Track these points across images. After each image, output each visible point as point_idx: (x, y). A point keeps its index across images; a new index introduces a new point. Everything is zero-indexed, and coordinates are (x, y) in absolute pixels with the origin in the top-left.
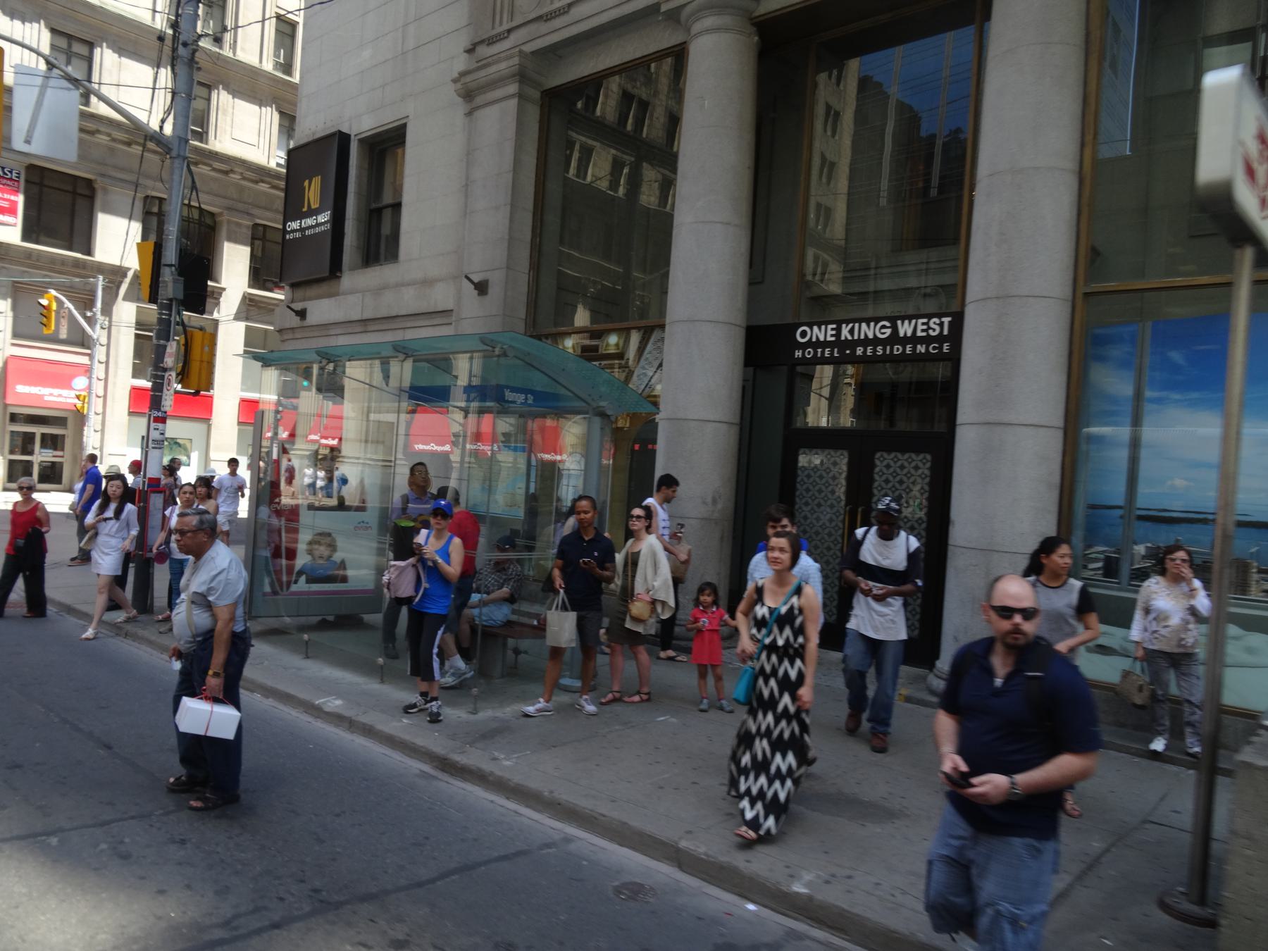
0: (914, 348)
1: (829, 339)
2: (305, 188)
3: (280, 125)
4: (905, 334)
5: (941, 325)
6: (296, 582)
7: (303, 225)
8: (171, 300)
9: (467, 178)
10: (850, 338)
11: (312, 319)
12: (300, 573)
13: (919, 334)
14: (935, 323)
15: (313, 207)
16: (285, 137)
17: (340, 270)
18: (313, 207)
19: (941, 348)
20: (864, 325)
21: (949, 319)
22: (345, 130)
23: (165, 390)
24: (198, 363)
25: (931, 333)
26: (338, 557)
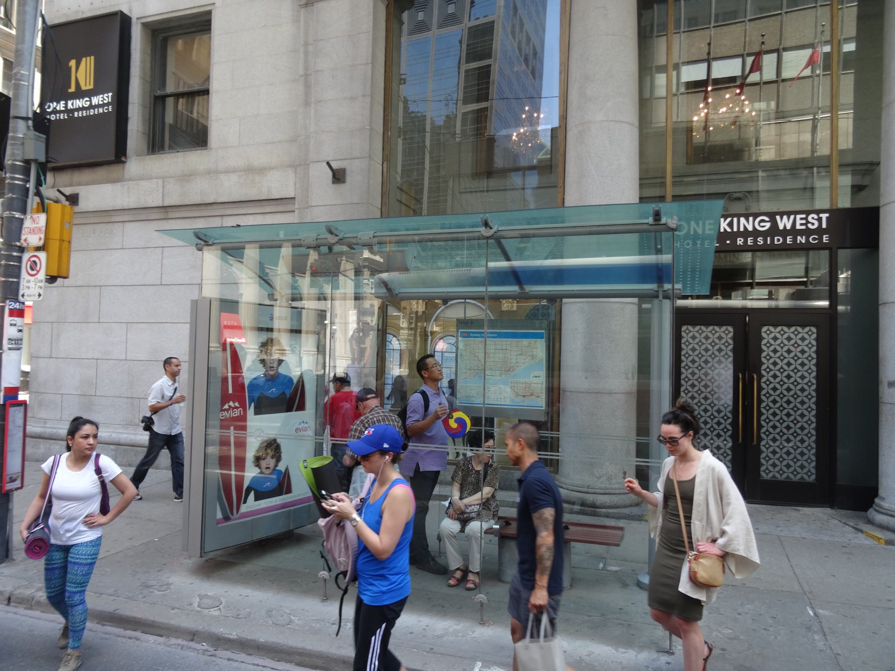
0: (795, 239)
1: (707, 232)
2: (70, 68)
5: (820, 220)
7: (70, 106)
8: (27, 162)
9: (306, 68)
10: (729, 230)
11: (85, 204)
12: (249, 490)
13: (798, 227)
14: (813, 218)
17: (125, 155)
19: (821, 239)
20: (742, 220)
21: (827, 215)
23: (24, 274)
24: (57, 243)
25: (810, 226)
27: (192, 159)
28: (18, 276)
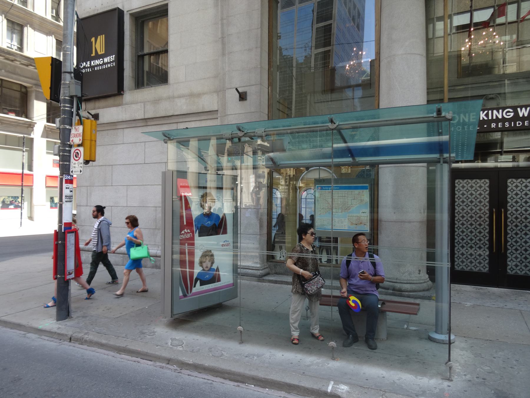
1: (471, 120)
2: (92, 42)
3: (8, 26)
4: (524, 114)
6: (195, 286)
8: (72, 97)
9: (223, 33)
10: (486, 118)
15: (99, 53)
16: (10, 34)
17: (123, 90)
18: (99, 53)
20: (495, 112)
22: (121, 8)
23: (72, 160)
26: (214, 267)
27: (159, 91)
28: (69, 161)
